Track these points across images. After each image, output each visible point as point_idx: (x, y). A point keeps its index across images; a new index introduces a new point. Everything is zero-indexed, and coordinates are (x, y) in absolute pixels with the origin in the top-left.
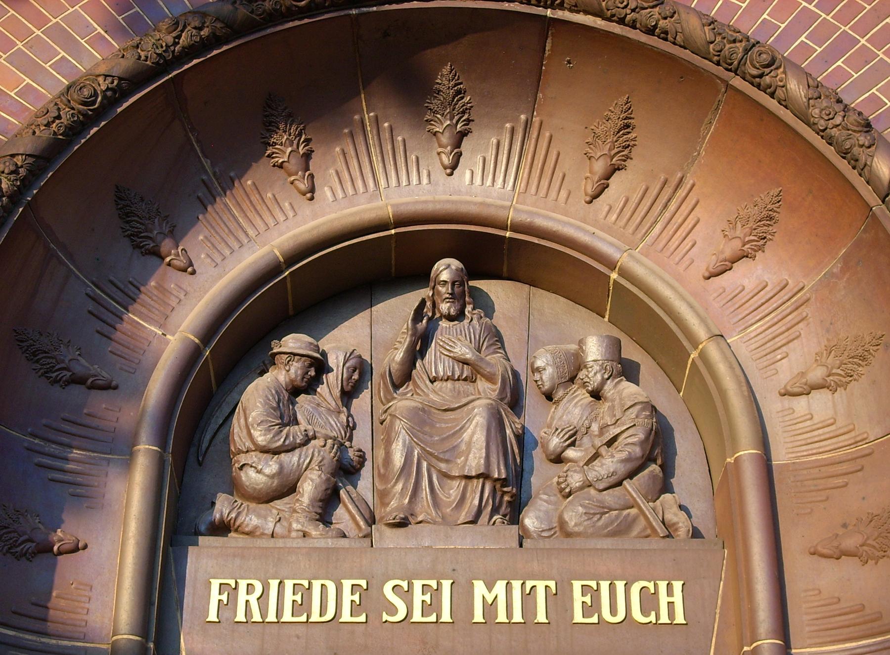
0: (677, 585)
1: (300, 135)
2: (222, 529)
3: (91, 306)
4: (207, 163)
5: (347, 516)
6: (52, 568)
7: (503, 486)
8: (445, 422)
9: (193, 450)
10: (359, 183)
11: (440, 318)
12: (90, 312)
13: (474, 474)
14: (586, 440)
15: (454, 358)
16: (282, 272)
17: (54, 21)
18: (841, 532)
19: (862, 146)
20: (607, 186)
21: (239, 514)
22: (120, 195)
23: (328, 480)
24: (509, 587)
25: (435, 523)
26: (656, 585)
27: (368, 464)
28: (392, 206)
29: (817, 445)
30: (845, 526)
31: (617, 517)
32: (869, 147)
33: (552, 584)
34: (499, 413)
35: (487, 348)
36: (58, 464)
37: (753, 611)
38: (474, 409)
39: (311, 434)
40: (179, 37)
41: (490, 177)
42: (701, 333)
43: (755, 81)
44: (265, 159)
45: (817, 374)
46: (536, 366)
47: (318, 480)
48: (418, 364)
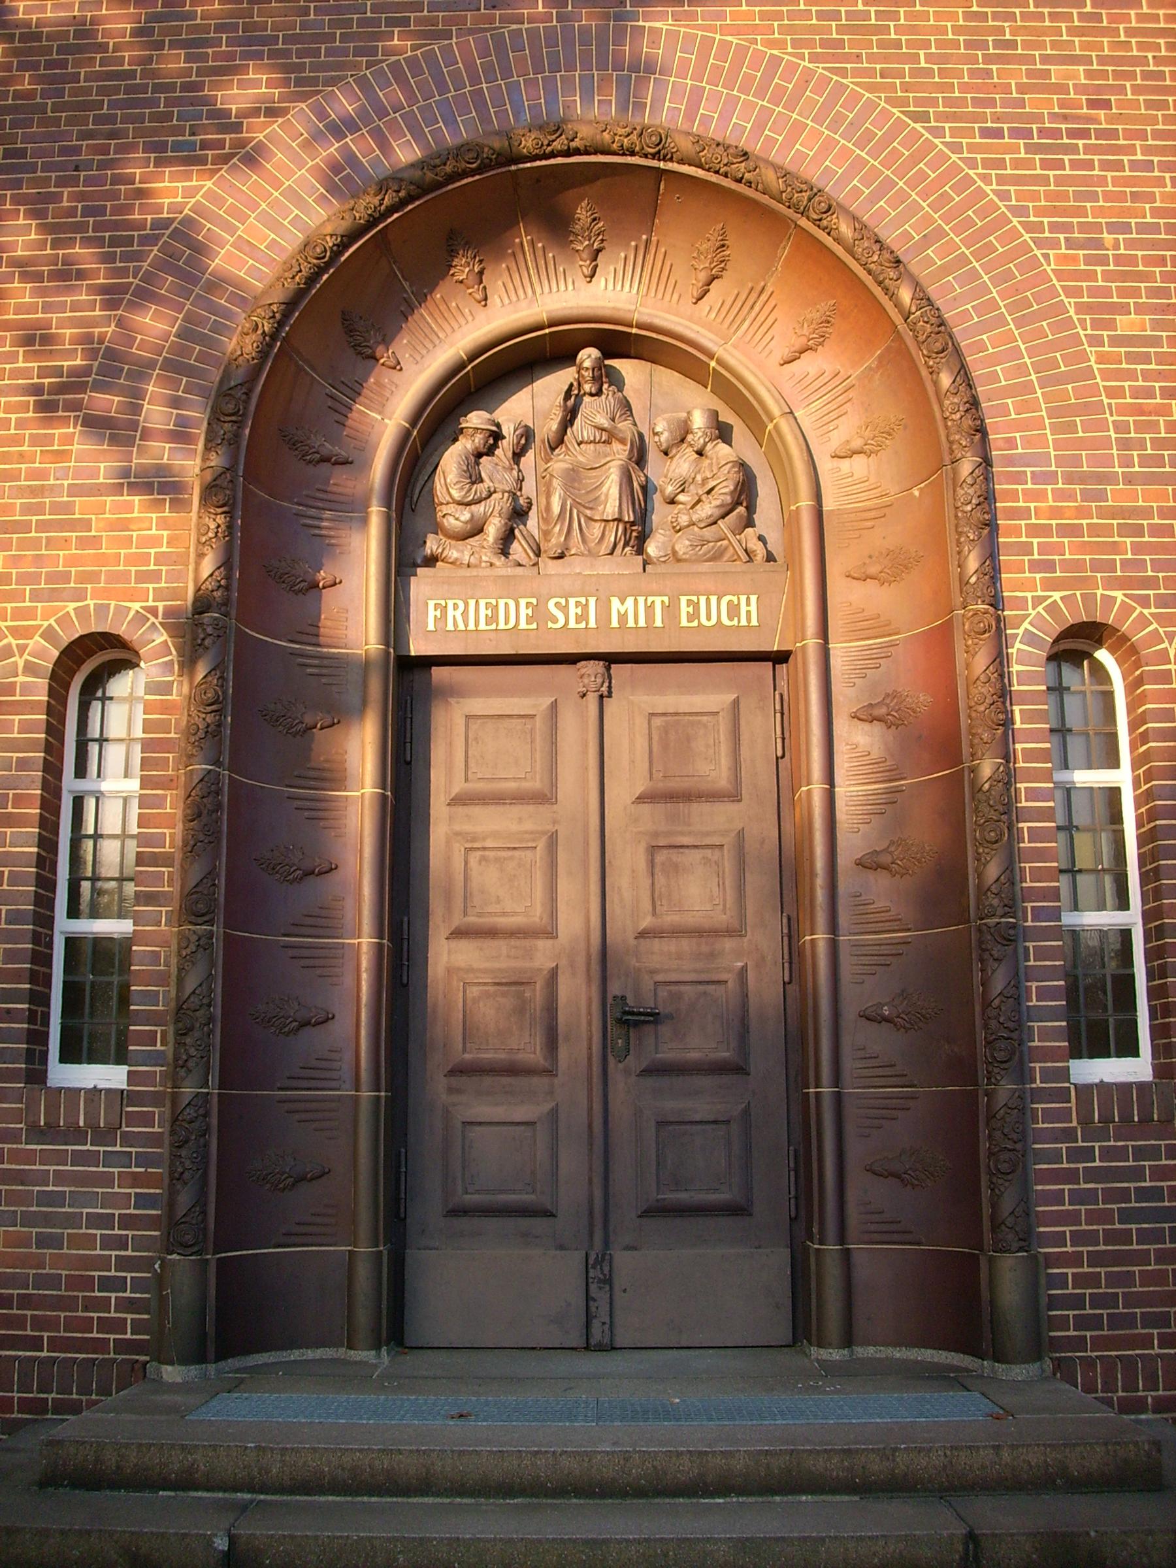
0: (754, 598)
1: (475, 257)
2: (431, 561)
3: (330, 403)
4: (406, 285)
5: (520, 549)
6: (319, 599)
7: (631, 526)
8: (590, 480)
9: (408, 500)
10: (521, 292)
11: (585, 394)
12: (330, 407)
13: (610, 518)
14: (692, 487)
15: (595, 427)
16: (465, 367)
17: (287, 183)
18: (868, 561)
19: (891, 279)
20: (709, 290)
21: (443, 550)
22: (345, 317)
23: (506, 523)
24: (636, 601)
25: (583, 555)
26: (739, 599)
27: (534, 508)
28: (547, 312)
29: (855, 496)
30: (870, 557)
31: (713, 547)
32: (897, 280)
33: (666, 599)
34: (629, 471)
35: (620, 416)
36: (316, 523)
37: (803, 619)
38: (610, 468)
39: (492, 489)
40: (383, 199)
41: (620, 283)
42: (775, 410)
43: (817, 222)
44: (449, 277)
45: (857, 443)
46: (656, 431)
47: (499, 525)
48: (569, 430)
